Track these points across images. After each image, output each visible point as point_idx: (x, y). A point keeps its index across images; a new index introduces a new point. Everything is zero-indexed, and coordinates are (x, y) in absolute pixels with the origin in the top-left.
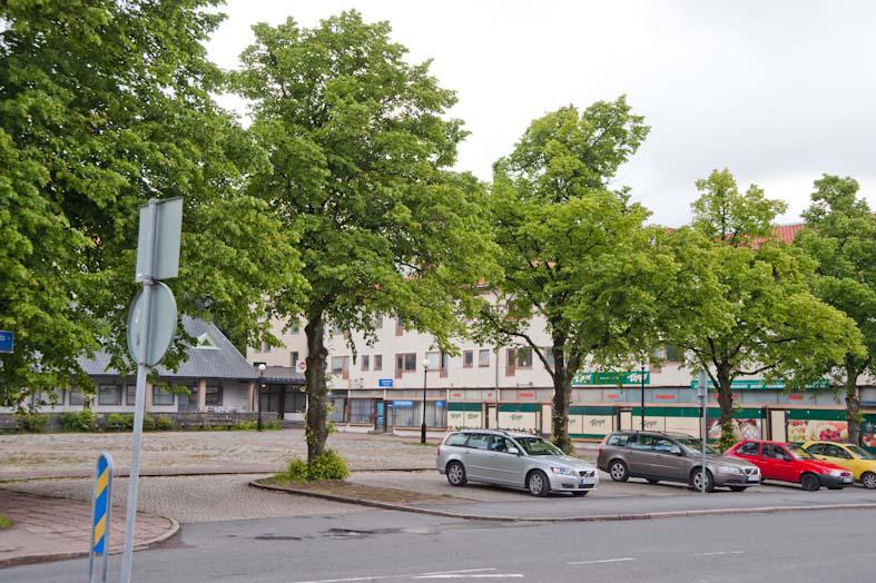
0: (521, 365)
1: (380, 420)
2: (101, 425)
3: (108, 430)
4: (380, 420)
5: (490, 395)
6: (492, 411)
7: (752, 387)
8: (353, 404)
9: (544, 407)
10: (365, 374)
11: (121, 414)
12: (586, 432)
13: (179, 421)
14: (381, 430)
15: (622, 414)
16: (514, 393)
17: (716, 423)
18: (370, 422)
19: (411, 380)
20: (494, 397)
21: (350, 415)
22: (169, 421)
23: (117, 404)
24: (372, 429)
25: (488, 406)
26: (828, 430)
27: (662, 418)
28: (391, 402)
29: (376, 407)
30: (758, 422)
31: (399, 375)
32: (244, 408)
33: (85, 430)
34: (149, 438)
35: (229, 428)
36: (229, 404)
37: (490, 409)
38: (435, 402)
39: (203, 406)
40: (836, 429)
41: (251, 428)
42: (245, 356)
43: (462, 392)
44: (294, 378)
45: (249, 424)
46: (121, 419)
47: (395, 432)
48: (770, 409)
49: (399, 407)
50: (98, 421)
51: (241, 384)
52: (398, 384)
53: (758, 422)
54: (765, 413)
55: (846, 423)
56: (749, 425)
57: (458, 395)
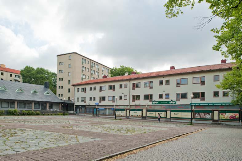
0: (136, 99)
1: (95, 113)
2: (20, 114)
3: (22, 115)
4: (95, 113)
5: (127, 107)
6: (128, 111)
7: (209, 105)
8: (87, 109)
9: (143, 110)
10: (90, 102)
11: (26, 111)
12: (182, 117)
13: (42, 113)
14: (95, 115)
15: (167, 112)
16: (134, 106)
17: (197, 114)
18: (92, 113)
19: (103, 103)
20: (129, 107)
21: (86, 112)
22: (39, 113)
23: (24, 108)
24: (93, 115)
25: (127, 109)
26: (232, 116)
27: (180, 113)
28: (98, 109)
29: (94, 110)
30: (210, 114)
31: (100, 102)
32: (59, 110)
33: (15, 115)
34: (66, 119)
35: (56, 115)
36: (55, 109)
37: (127, 110)
38: (111, 108)
39: (48, 109)
40: (234, 115)
41: (61, 115)
42: (56, 95)
43: (119, 106)
44: (71, 102)
45: (61, 114)
46: (26, 112)
47: (99, 116)
48: (214, 110)
49: (100, 110)
50: (19, 112)
51: (58, 103)
52: (100, 104)
53: (210, 114)
54: (212, 112)
55: (238, 114)
56: (207, 115)
57: (151, 107)
